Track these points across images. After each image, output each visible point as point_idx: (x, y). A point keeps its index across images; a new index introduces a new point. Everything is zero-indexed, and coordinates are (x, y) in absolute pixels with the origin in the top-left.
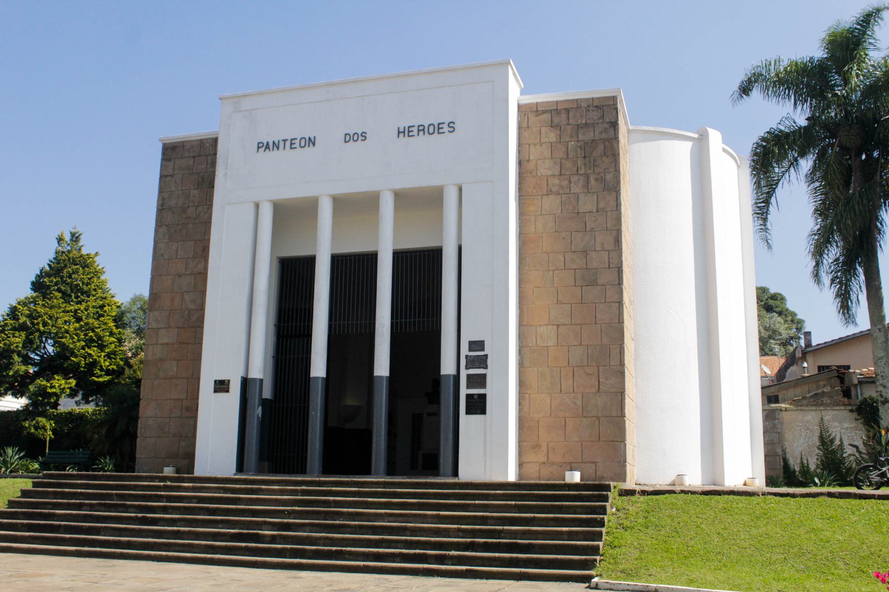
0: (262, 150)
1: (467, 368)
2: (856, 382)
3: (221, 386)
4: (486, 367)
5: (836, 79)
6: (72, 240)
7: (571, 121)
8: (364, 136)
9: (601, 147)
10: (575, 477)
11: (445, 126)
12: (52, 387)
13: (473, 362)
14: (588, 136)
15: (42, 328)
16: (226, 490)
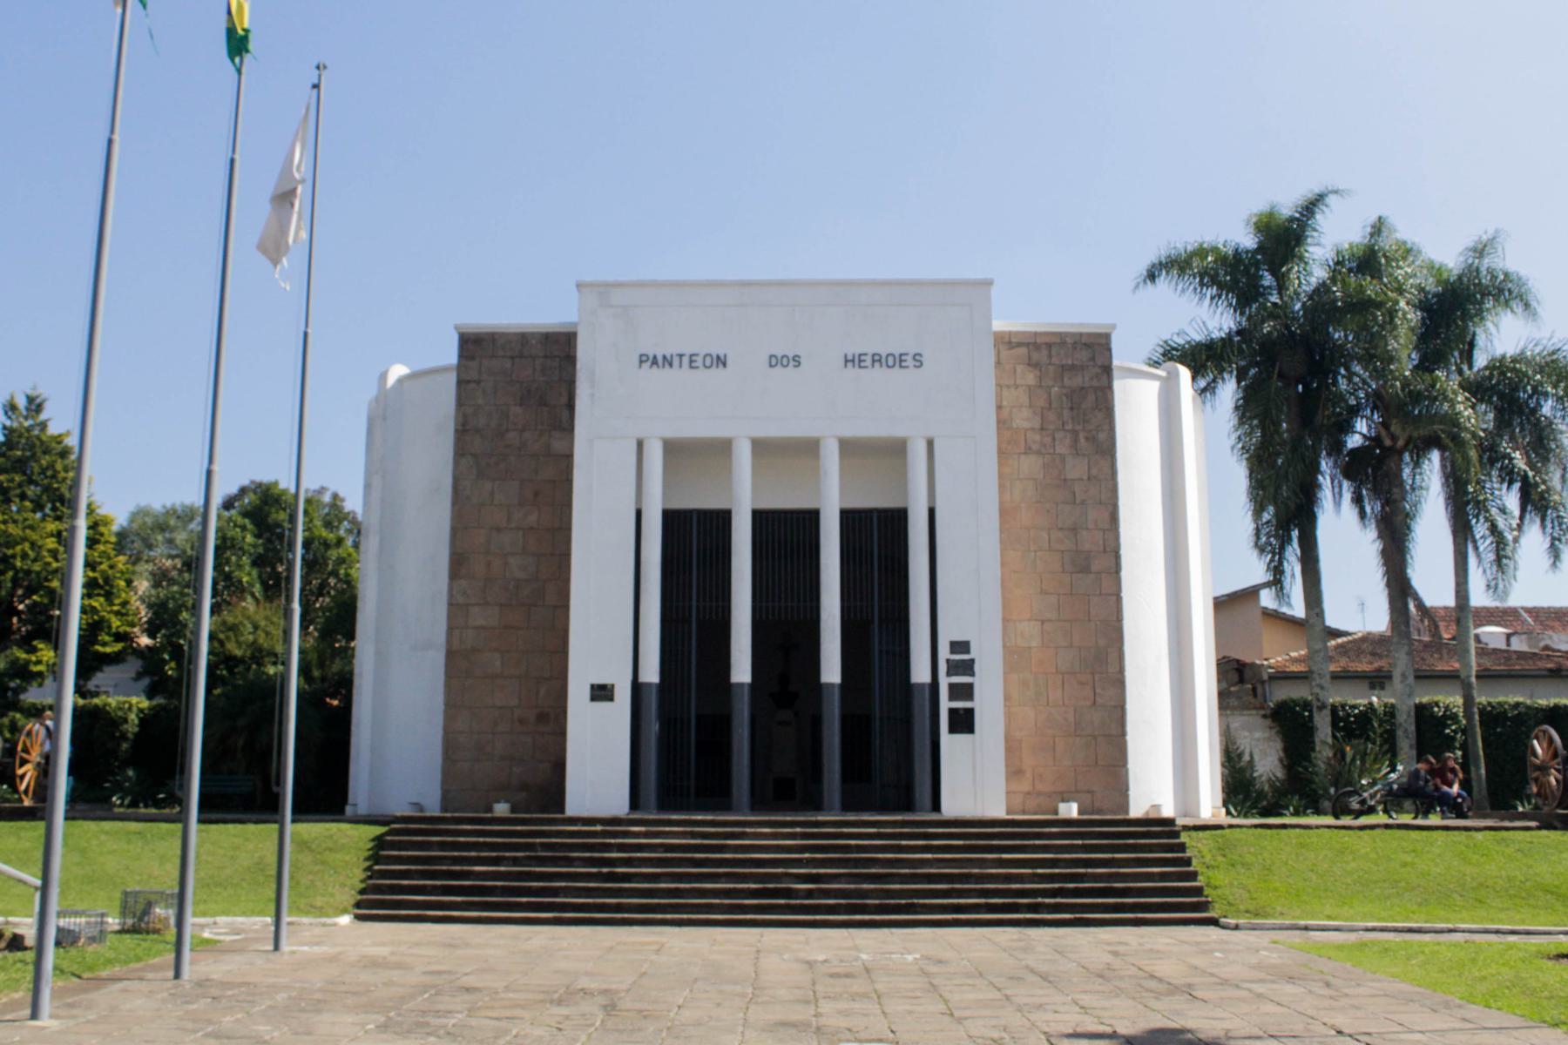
0: (646, 365)
1: (949, 674)
2: (1265, 677)
3: (601, 693)
4: (973, 674)
5: (1268, 280)
6: (27, 409)
7: (1054, 360)
8: (797, 361)
9: (1091, 398)
10: (1071, 810)
11: (909, 358)
12: (39, 662)
13: (954, 668)
14: (1077, 381)
15: (18, 564)
16: (693, 835)
